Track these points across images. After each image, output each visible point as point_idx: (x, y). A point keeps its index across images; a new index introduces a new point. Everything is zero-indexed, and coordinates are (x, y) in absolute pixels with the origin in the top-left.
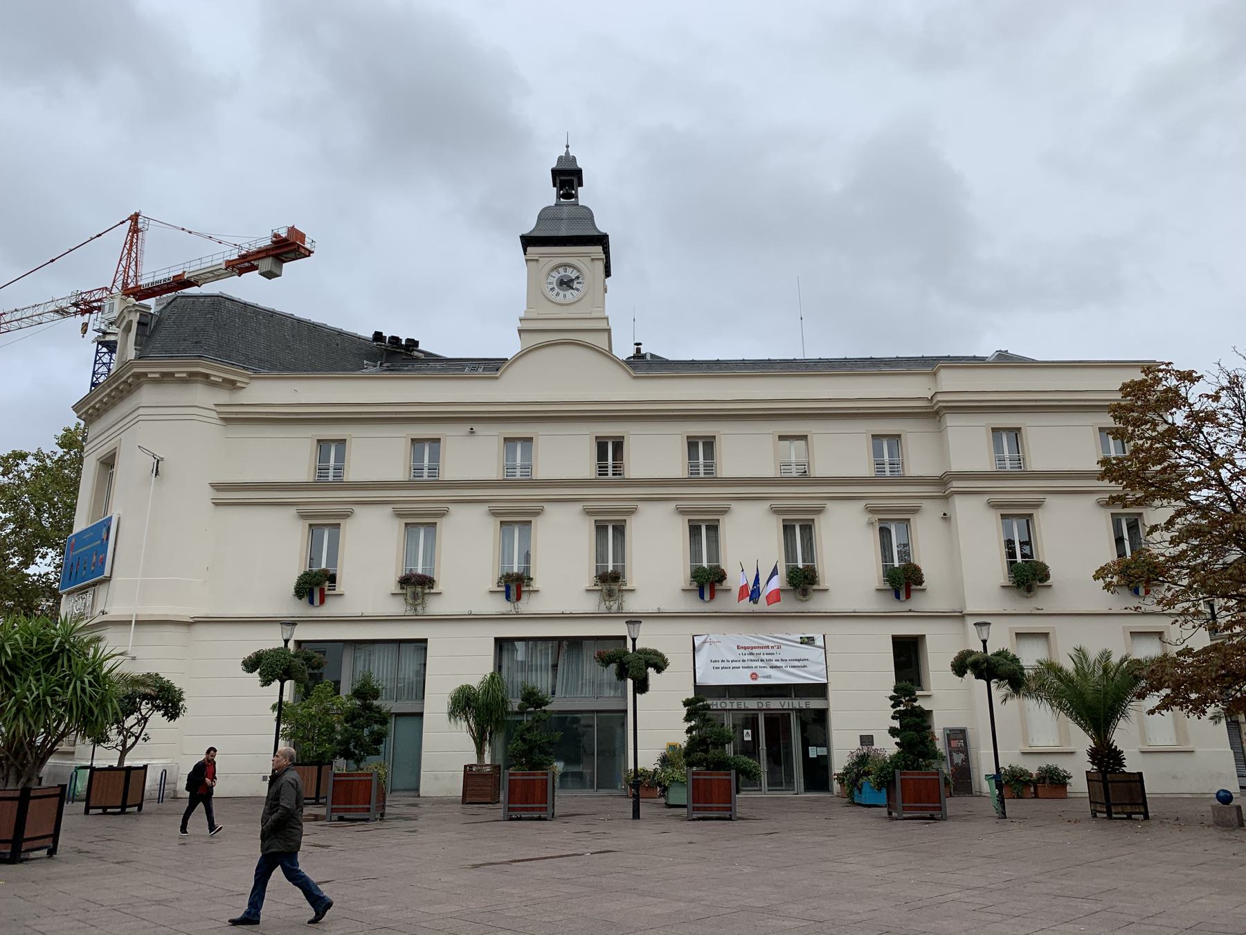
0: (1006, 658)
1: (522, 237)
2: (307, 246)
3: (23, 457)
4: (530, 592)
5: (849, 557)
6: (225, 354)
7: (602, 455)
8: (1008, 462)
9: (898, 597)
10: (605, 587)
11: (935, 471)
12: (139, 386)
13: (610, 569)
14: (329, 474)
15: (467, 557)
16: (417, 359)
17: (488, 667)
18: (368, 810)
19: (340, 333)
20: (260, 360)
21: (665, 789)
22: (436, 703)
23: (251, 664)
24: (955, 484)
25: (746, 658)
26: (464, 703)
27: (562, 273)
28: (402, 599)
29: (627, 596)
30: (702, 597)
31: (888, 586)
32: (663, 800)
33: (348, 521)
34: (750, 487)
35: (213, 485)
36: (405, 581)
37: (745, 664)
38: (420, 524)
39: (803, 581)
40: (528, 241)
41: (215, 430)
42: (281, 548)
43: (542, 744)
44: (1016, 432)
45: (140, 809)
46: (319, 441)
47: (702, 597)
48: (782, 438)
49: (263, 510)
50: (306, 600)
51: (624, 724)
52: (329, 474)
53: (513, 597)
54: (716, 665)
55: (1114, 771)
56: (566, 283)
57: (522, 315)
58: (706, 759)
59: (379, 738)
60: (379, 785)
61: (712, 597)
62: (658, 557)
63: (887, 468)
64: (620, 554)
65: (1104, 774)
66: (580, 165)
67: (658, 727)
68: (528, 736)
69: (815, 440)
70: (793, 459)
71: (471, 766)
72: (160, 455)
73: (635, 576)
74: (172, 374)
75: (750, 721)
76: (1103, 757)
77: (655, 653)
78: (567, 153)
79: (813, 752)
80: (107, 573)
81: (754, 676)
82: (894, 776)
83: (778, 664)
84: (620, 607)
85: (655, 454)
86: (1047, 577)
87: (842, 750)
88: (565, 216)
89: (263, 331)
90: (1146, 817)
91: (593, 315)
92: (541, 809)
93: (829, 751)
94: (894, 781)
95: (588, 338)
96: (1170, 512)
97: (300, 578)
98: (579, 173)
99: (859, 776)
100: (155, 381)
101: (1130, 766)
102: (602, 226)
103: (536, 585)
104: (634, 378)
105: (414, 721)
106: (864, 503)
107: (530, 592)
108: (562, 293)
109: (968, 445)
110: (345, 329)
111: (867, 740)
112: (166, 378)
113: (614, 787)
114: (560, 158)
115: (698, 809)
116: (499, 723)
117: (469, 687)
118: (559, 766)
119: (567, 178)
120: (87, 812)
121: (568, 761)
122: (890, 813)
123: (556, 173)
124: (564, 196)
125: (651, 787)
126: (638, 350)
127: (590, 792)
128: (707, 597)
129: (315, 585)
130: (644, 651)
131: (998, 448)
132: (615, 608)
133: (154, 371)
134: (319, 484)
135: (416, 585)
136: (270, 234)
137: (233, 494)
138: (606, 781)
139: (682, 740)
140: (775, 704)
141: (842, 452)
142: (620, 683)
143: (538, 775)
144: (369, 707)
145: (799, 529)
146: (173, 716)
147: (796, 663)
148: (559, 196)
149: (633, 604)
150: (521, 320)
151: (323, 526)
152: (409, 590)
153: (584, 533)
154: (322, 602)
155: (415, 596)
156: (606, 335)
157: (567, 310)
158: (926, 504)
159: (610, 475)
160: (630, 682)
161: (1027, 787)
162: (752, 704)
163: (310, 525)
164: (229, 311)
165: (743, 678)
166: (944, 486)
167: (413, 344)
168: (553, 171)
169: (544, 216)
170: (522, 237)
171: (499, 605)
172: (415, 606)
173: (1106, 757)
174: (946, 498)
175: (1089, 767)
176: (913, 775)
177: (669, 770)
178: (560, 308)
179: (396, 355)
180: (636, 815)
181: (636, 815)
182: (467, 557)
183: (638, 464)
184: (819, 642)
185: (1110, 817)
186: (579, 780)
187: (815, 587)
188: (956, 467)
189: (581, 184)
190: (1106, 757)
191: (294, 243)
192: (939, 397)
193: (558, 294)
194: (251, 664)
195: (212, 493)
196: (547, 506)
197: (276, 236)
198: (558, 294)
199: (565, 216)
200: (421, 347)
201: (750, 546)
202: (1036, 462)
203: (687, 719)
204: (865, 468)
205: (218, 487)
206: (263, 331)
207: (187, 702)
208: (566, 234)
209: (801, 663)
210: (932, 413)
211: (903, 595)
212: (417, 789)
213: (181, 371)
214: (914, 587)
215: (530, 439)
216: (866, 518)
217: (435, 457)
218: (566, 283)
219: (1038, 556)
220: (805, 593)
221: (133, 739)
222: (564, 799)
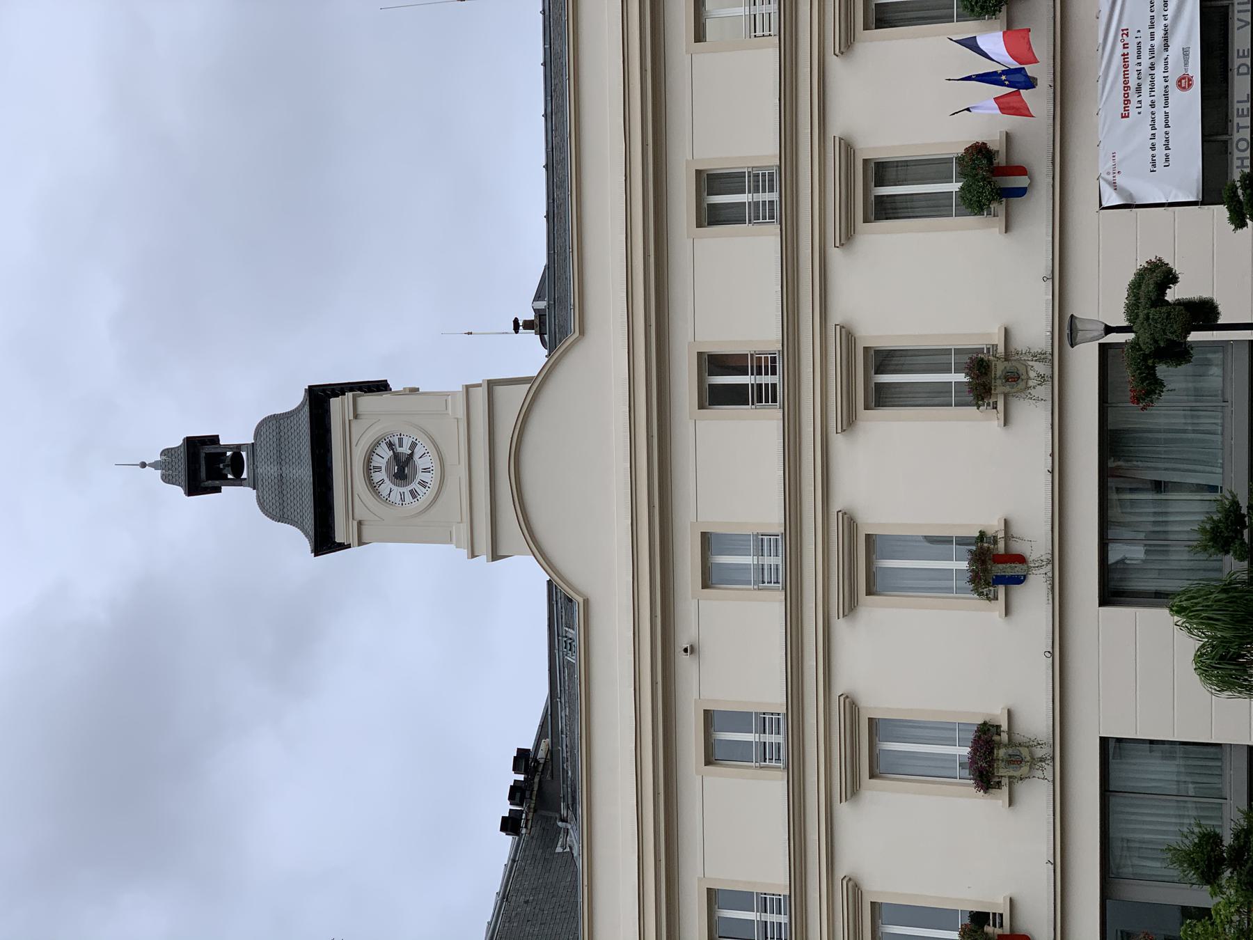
7: (736, 396)
10: (1000, 388)
13: (962, 377)
15: (935, 659)
16: (551, 752)
17: (1160, 619)
30: (1021, 192)
36: (985, 779)
37: (1160, 103)
40: (324, 542)
48: (700, 36)
53: (1017, 569)
54: (1160, 161)
56: (401, 469)
57: (464, 552)
61: (1022, 171)
62: (936, 283)
64: (932, 359)
66: (177, 442)
73: (976, 328)
77: (1135, 286)
78: (155, 465)
81: (1184, 83)
84: (1040, 357)
85: (733, 290)
91: (461, 413)
95: (507, 425)
98: (193, 444)
102: (294, 399)
103: (993, 525)
104: (582, 332)
107: (1008, 536)
108: (421, 476)
114: (167, 479)
117: (1199, 656)
119: (203, 465)
123: (194, 488)
124: (238, 471)
126: (528, 325)
128: (1021, 182)
132: (1041, 368)
135: (992, 758)
142: (1196, 355)
148: (238, 481)
149: (1035, 332)
150: (473, 556)
152: (1003, 771)
155: (1015, 761)
156: (500, 390)
157: (451, 461)
160: (1194, 336)
167: (522, 760)
169: (276, 509)
171: (1034, 598)
172: (1035, 762)
182: (935, 659)
183: (751, 325)
189: (214, 440)
196: (837, 504)
198: (423, 484)
200: (529, 745)
217: (740, 720)
218: (401, 469)
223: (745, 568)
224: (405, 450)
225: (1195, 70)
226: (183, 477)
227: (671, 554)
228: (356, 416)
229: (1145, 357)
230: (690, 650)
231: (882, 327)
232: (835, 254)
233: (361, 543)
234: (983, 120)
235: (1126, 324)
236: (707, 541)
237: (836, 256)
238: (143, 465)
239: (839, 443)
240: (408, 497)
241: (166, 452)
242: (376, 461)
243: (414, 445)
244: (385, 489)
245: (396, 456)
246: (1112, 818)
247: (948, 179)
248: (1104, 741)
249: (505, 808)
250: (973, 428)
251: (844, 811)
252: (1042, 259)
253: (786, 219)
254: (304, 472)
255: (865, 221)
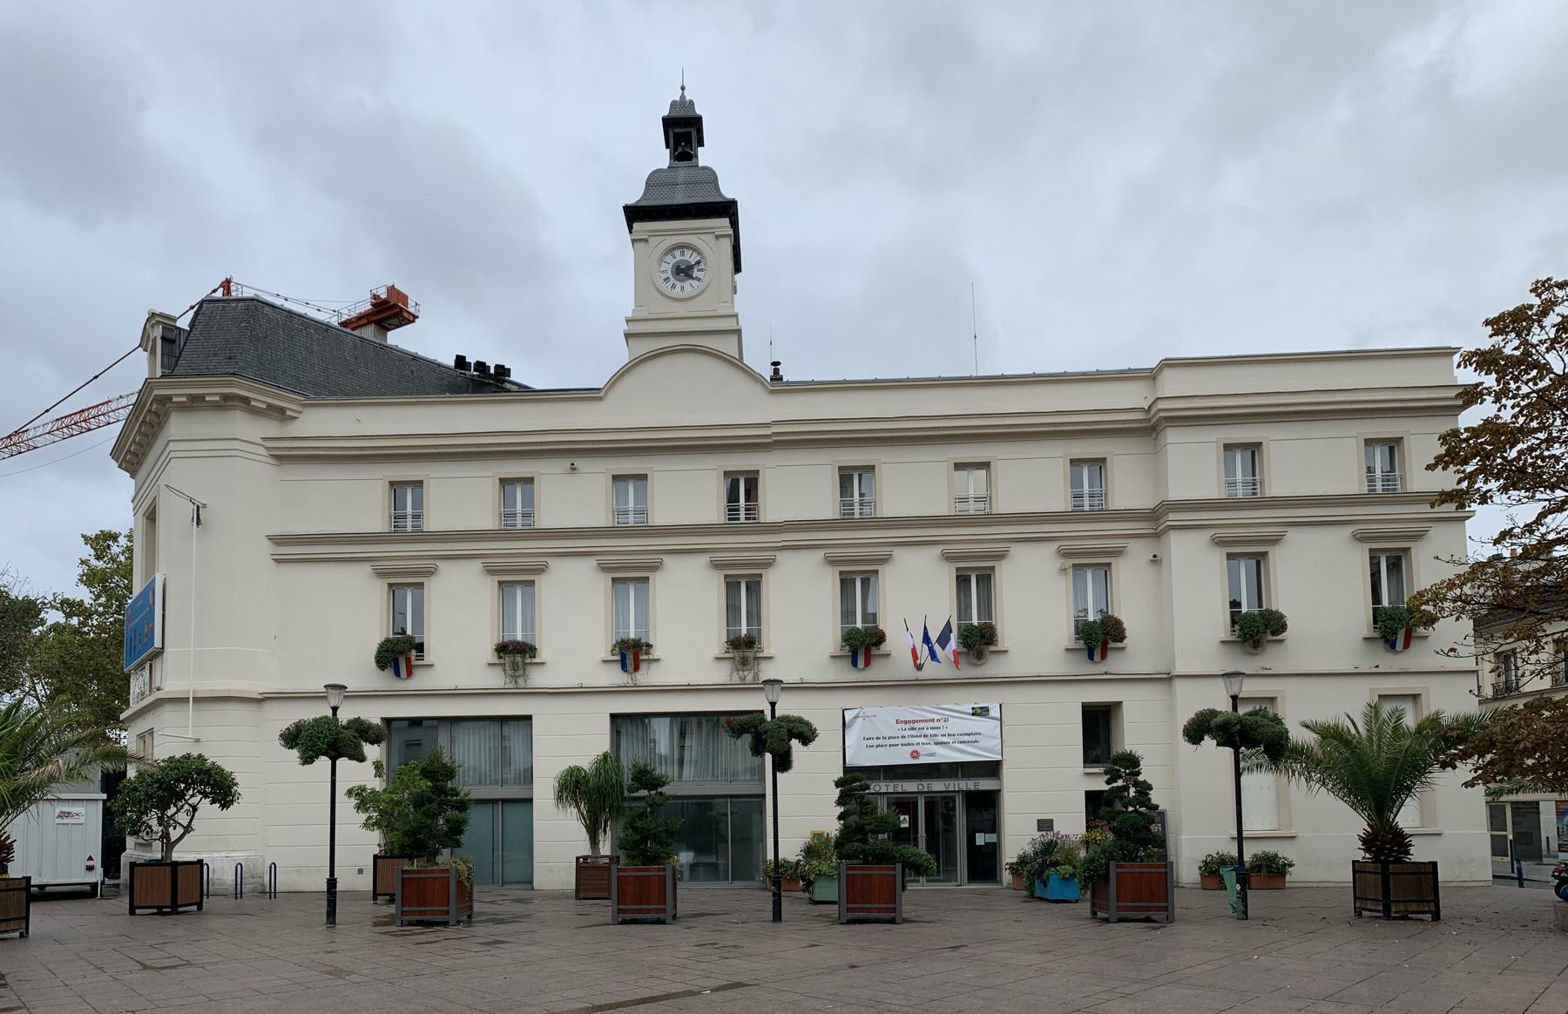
0: (1264, 716)
1: (627, 209)
2: (412, 310)
3: (114, 537)
4: (650, 661)
5: (1035, 609)
6: (268, 374)
7: (733, 497)
8: (1239, 486)
9: (1091, 657)
10: (737, 654)
11: (1146, 502)
12: (167, 416)
13: (744, 632)
14: (405, 519)
15: (574, 622)
17: (603, 744)
18: (447, 913)
19: (415, 358)
20: (315, 385)
21: (809, 883)
22: (544, 789)
23: (291, 738)
24: (1172, 516)
25: (906, 733)
26: (574, 787)
27: (679, 258)
28: (499, 669)
29: (764, 665)
30: (855, 664)
31: (1081, 644)
32: (807, 895)
33: (432, 579)
34: (917, 529)
35: (271, 538)
36: (503, 649)
37: (905, 741)
38: (515, 581)
39: (978, 641)
40: (634, 214)
41: (266, 471)
42: (353, 614)
43: (667, 830)
44: (1254, 449)
45: (200, 907)
46: (391, 483)
47: (855, 664)
48: (959, 466)
49: (333, 565)
50: (389, 672)
51: (762, 812)
52: (405, 519)
53: (630, 667)
54: (870, 743)
55: (1399, 861)
56: (683, 271)
57: (630, 315)
58: (863, 851)
59: (456, 828)
60: (460, 883)
61: (867, 664)
62: (801, 619)
63: (1086, 502)
64: (755, 615)
65: (1385, 865)
66: (698, 112)
67: (804, 809)
68: (638, 824)
69: (999, 469)
70: (972, 493)
71: (585, 858)
72: (201, 499)
73: (774, 640)
74: (201, 398)
75: (905, 804)
76: (1384, 843)
77: (800, 720)
78: (683, 97)
79: (980, 839)
80: (158, 644)
81: (915, 754)
82: (1108, 869)
83: (944, 739)
84: (756, 676)
85: (797, 490)
86: (1283, 627)
87: (1017, 837)
88: (680, 180)
89: (316, 348)
90: (1436, 916)
91: (720, 312)
92: (658, 911)
93: (999, 838)
94: (1106, 878)
95: (712, 343)
96: (1538, 508)
97: (381, 646)
98: (697, 122)
99: (1044, 867)
100: (182, 407)
101: (1419, 853)
102: (728, 192)
103: (656, 653)
104: (772, 392)
105: (523, 806)
106: (1055, 545)
107: (650, 661)
108: (678, 284)
109: (1194, 467)
110: (422, 353)
111: (1046, 825)
112: (195, 403)
113: (751, 878)
114: (673, 104)
115: (853, 910)
116: (616, 811)
117: (579, 769)
118: (685, 857)
119: (683, 131)
120: (132, 912)
121: (699, 850)
122: (1094, 913)
123: (668, 123)
125: (793, 879)
126: (776, 371)
127: (723, 884)
128: (861, 664)
129: (399, 654)
130: (786, 719)
131: (1229, 468)
132: (750, 678)
133: (179, 393)
134: (397, 534)
135: (515, 653)
136: (368, 296)
137: (296, 549)
138: (742, 871)
139: (833, 827)
140: (938, 786)
141: (1033, 482)
142: (757, 760)
143: (653, 871)
144: (440, 791)
145: (974, 580)
146: (225, 805)
147: (967, 738)
149: (768, 672)
150: (627, 321)
151: (404, 585)
152: (508, 659)
153: (714, 589)
154: (409, 674)
155: (515, 667)
156: (735, 338)
157: (690, 305)
158: (1133, 546)
159: (742, 520)
160: (768, 757)
161: (1253, 875)
162: (910, 786)
163: (390, 585)
164: (270, 321)
165: (902, 758)
166: (1157, 521)
167: (502, 371)
168: (665, 120)
169: (655, 180)
170: (627, 209)
171: (614, 676)
172: (515, 678)
173: (1385, 844)
174: (1157, 536)
175: (1360, 855)
176: (1129, 868)
177: (815, 862)
178: (676, 304)
179: (486, 381)
180: (777, 916)
181: (777, 916)
182: (574, 622)
183: (775, 504)
184: (995, 712)
185: (1387, 915)
186: (714, 871)
187: (992, 648)
188: (1176, 493)
189: (701, 144)
190: (1385, 844)
191: (395, 306)
192: (1161, 405)
193: (674, 286)
194: (291, 738)
195: (269, 548)
196: (666, 559)
197: (375, 297)
198: (674, 286)
199: (680, 180)
200: (513, 378)
201: (916, 598)
202: (1276, 487)
203: (840, 802)
204: (1059, 502)
205: (278, 540)
206: (316, 348)
207: (244, 785)
208: (683, 204)
209: (972, 738)
210: (1148, 428)
211: (1097, 657)
212: (531, 882)
213: (213, 392)
214: (1112, 645)
215: (644, 477)
216: (1059, 562)
217: (529, 500)
218: (683, 271)
219: (1269, 602)
220: (980, 656)
221: (180, 830)
222: (689, 894)
223: (627, 503)
224: (696, 274)
225: (922, 760)
226: (675, 114)
227: (633, 453)
228: (717, 237)
229: (755, 727)
230: (573, 468)
231: (775, 587)
232: (820, 554)
233: (633, 241)
234: (900, 640)
235: (778, 714)
236: (643, 477)
237: (819, 555)
238: (683, 88)
239: (704, 559)
240: (664, 276)
241: (692, 103)
242: (688, 253)
243: (698, 279)
244: (669, 258)
245: (690, 267)
246: (481, 724)
247: (864, 621)
248: (529, 718)
249: (471, 359)
250: (714, 638)
251: (477, 565)
252: (813, 677)
253: (845, 522)
254: (679, 198)
255: (841, 573)
